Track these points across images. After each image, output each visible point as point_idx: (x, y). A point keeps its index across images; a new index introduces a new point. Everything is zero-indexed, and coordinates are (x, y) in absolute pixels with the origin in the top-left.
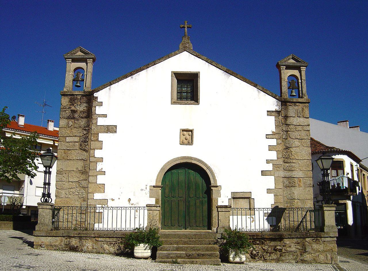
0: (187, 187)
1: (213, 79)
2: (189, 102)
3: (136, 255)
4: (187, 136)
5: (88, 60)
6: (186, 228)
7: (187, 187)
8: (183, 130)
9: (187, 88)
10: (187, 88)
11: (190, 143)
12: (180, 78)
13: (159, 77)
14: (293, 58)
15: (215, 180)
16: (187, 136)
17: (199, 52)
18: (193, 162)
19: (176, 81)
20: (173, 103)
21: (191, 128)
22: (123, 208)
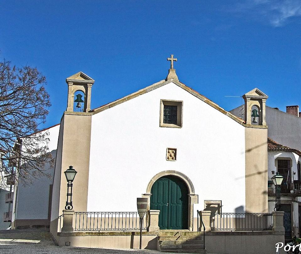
0: (171, 195)
1: (194, 107)
2: (172, 125)
3: (52, 184)
4: (173, 154)
5: (88, 84)
6: (169, 227)
7: (171, 195)
8: (169, 149)
9: (172, 113)
10: (172, 113)
11: (175, 158)
12: (167, 105)
13: (146, 105)
14: (257, 92)
15: (193, 190)
16: (173, 154)
17: (186, 82)
18: (175, 174)
19: (163, 106)
20: (180, 125)
21: (175, 148)
22: (113, 213)
